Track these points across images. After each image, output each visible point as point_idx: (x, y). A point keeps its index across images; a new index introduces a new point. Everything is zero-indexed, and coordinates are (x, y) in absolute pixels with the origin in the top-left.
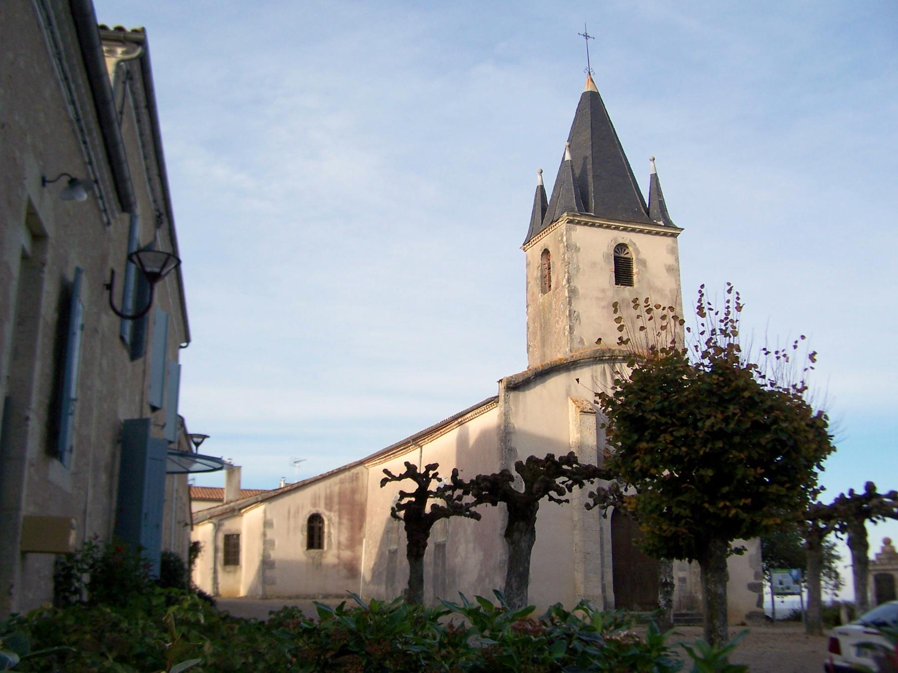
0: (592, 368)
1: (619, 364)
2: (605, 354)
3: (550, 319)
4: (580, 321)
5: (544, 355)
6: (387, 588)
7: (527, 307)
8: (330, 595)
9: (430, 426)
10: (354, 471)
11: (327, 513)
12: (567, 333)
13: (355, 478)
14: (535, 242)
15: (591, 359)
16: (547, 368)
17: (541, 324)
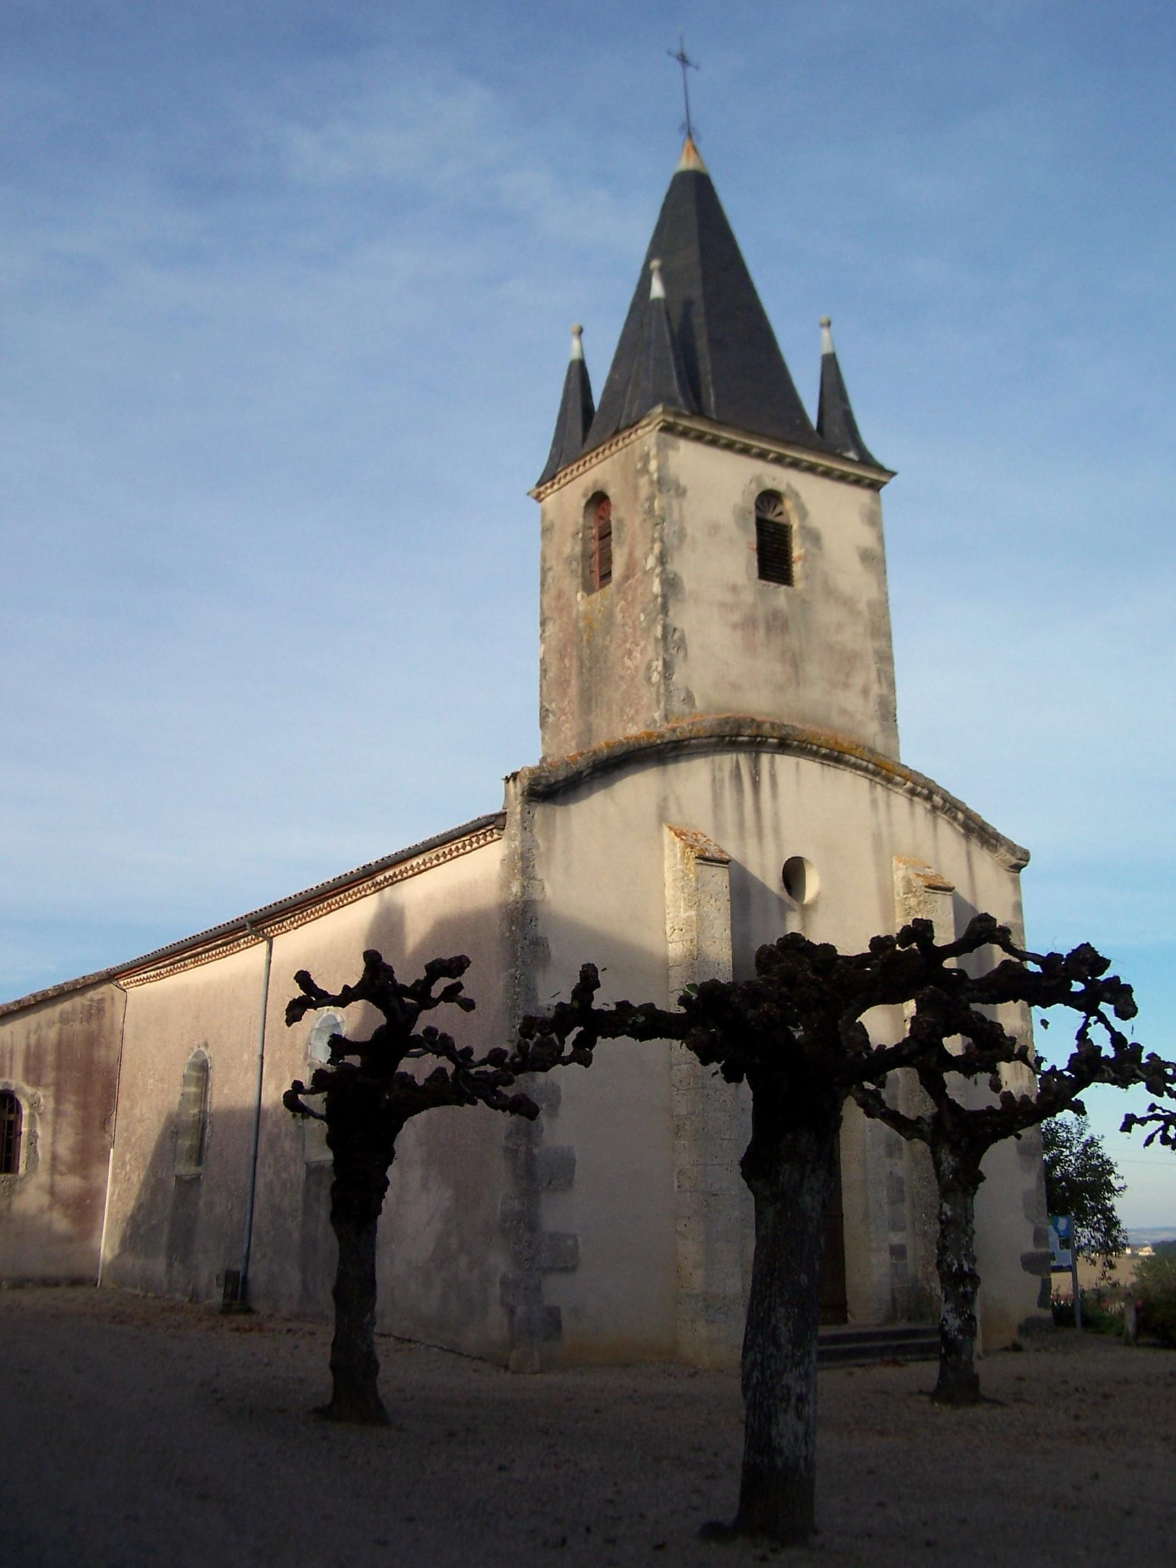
0: (713, 761)
1: (769, 756)
2: (742, 730)
3: (607, 648)
4: (686, 650)
5: (590, 730)
6: (170, 1265)
7: (543, 623)
8: (29, 1280)
9: (302, 890)
10: (92, 994)
11: (29, 1090)
12: (655, 677)
13: (97, 1011)
14: (569, 478)
15: (713, 740)
16: (619, 751)
17: (581, 661)
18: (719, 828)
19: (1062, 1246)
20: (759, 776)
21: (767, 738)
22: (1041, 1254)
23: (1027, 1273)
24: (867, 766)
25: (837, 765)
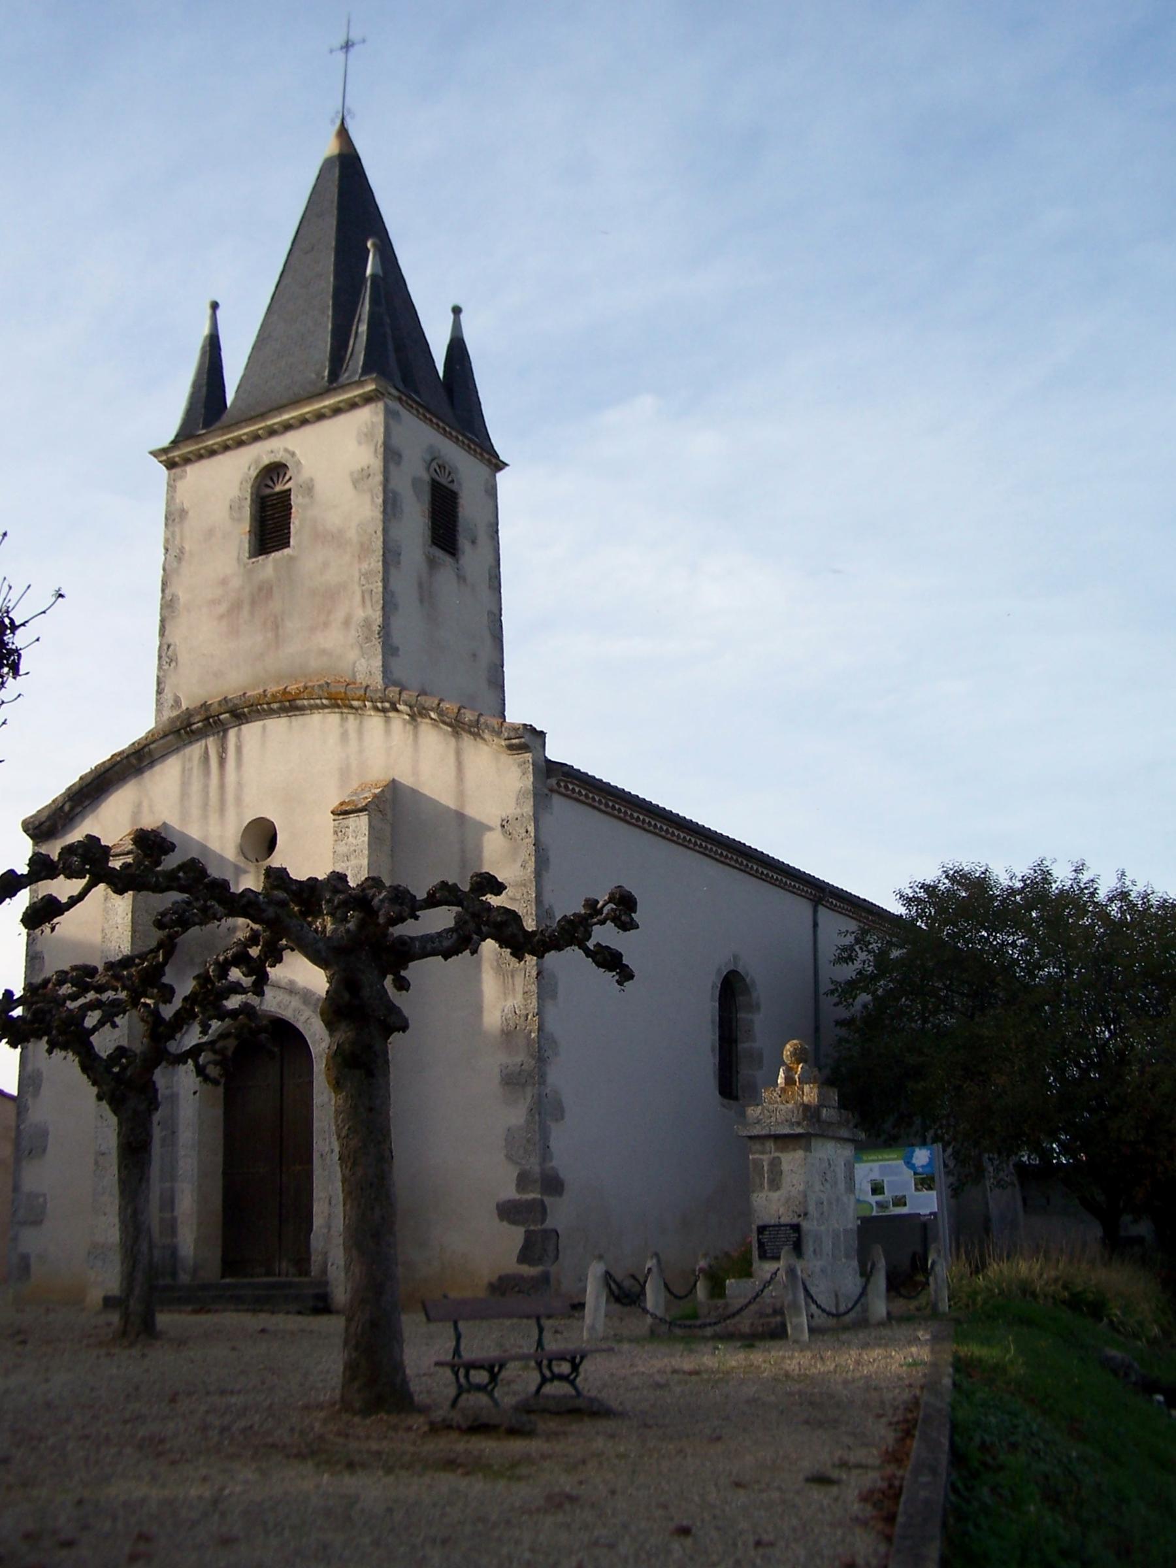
0: (184, 754)
4: (177, 663)
18: (184, 815)
19: (920, 1187)
20: (226, 754)
21: (218, 716)
22: (526, 1200)
23: (505, 1223)
24: (322, 703)
25: (302, 712)
